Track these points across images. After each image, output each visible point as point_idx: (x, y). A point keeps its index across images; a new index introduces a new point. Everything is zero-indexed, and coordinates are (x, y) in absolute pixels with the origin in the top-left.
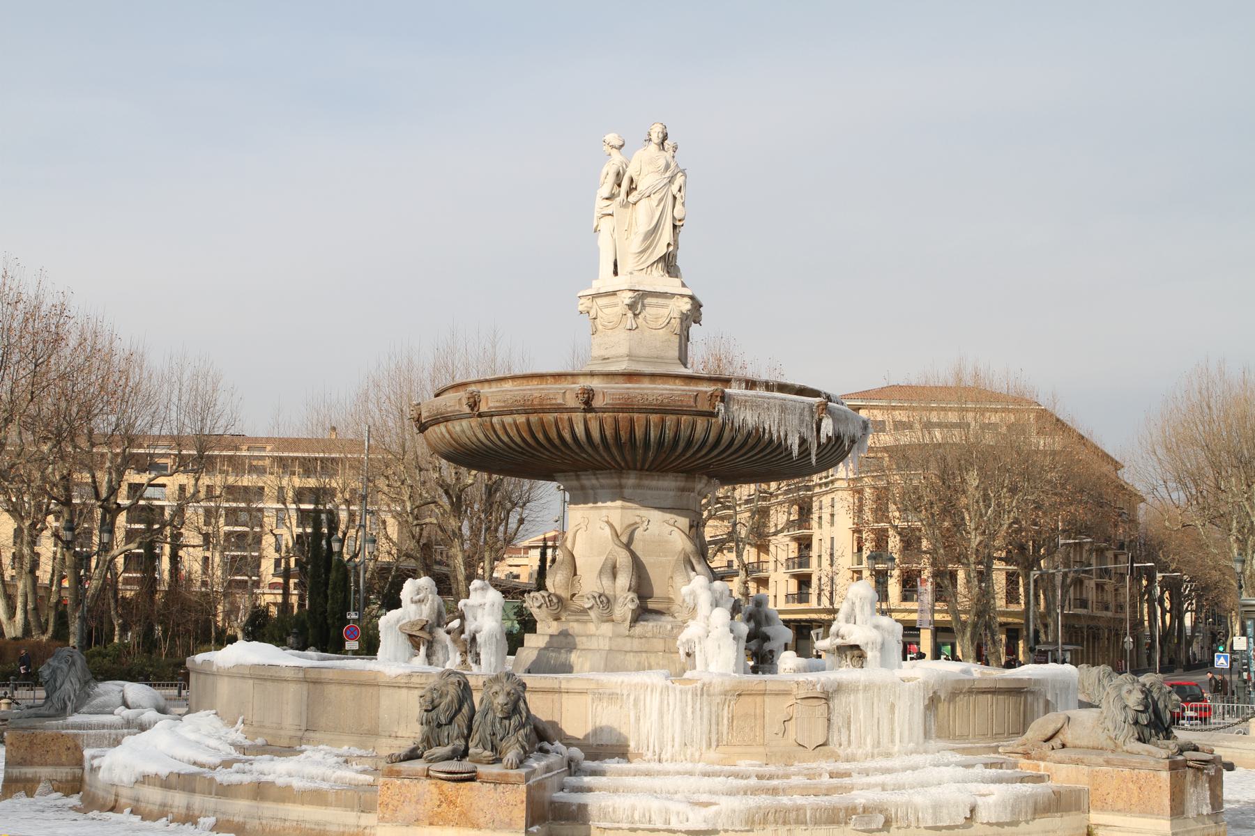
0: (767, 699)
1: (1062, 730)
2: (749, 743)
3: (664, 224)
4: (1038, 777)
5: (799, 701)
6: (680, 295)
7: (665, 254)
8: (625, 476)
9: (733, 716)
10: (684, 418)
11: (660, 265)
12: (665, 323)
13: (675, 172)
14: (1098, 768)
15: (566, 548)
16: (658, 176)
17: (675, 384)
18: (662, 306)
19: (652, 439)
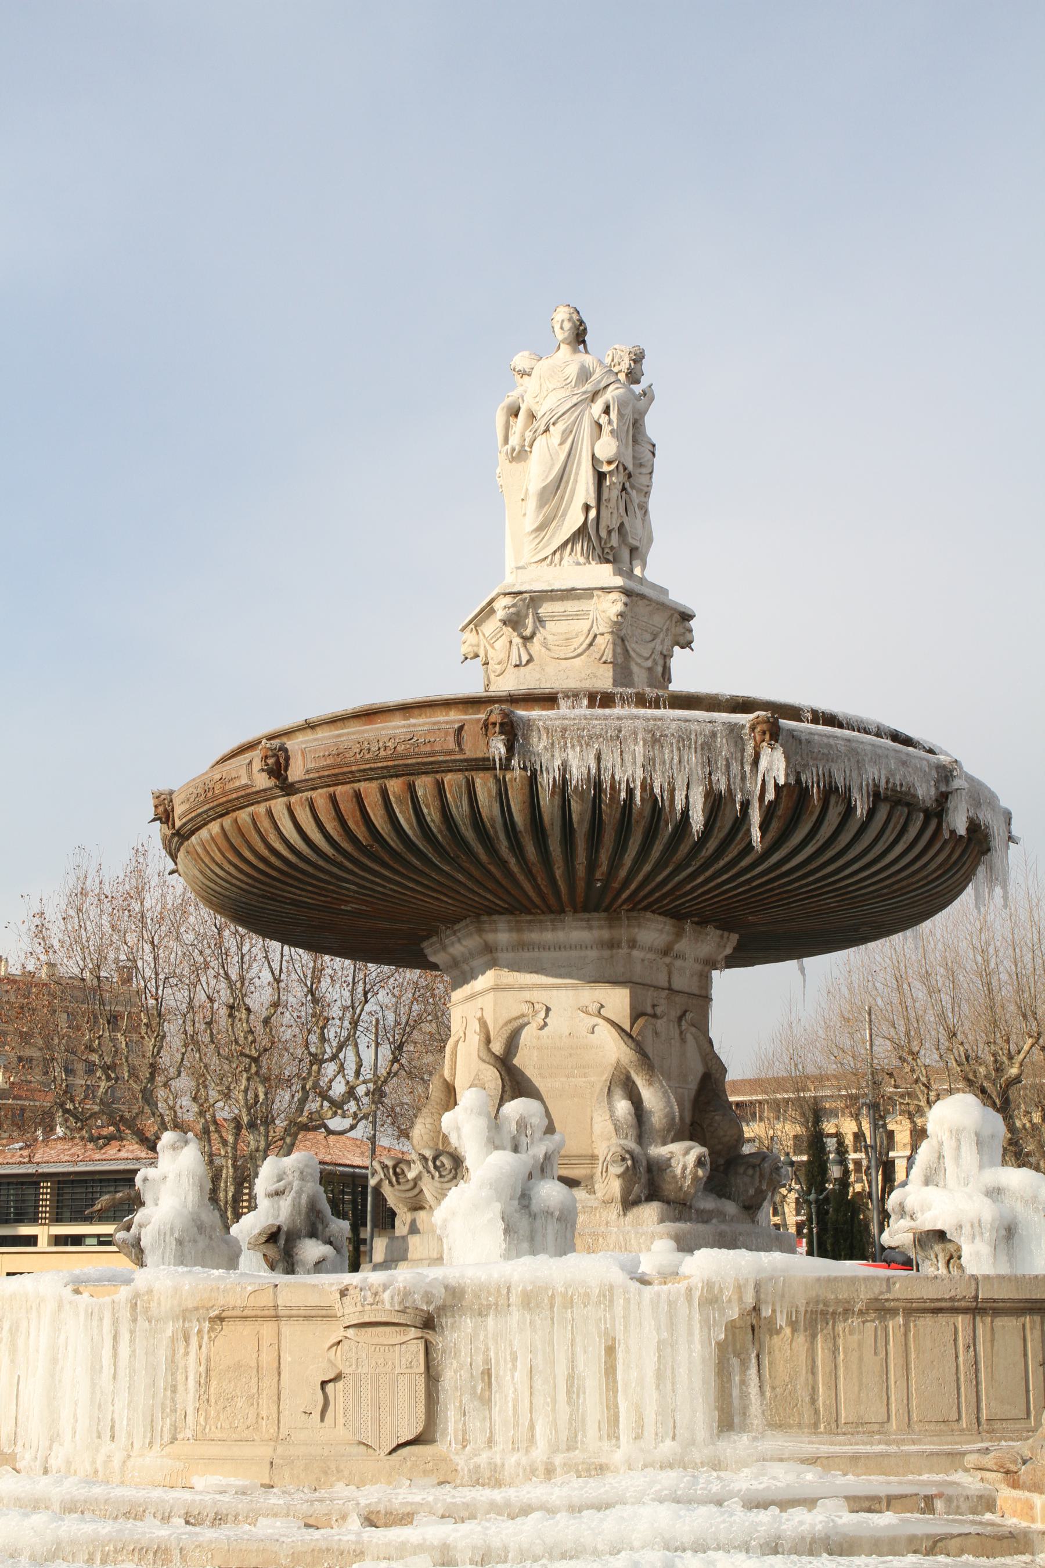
0: (288, 1329)
2: (246, 1434)
3: (577, 474)
4: (1000, 1538)
5: (351, 1332)
6: (602, 589)
8: (486, 926)
9: (208, 1370)
10: (448, 778)
11: (578, 547)
12: (584, 646)
13: (603, 384)
15: (442, 1076)
18: (577, 616)
19: (409, 832)
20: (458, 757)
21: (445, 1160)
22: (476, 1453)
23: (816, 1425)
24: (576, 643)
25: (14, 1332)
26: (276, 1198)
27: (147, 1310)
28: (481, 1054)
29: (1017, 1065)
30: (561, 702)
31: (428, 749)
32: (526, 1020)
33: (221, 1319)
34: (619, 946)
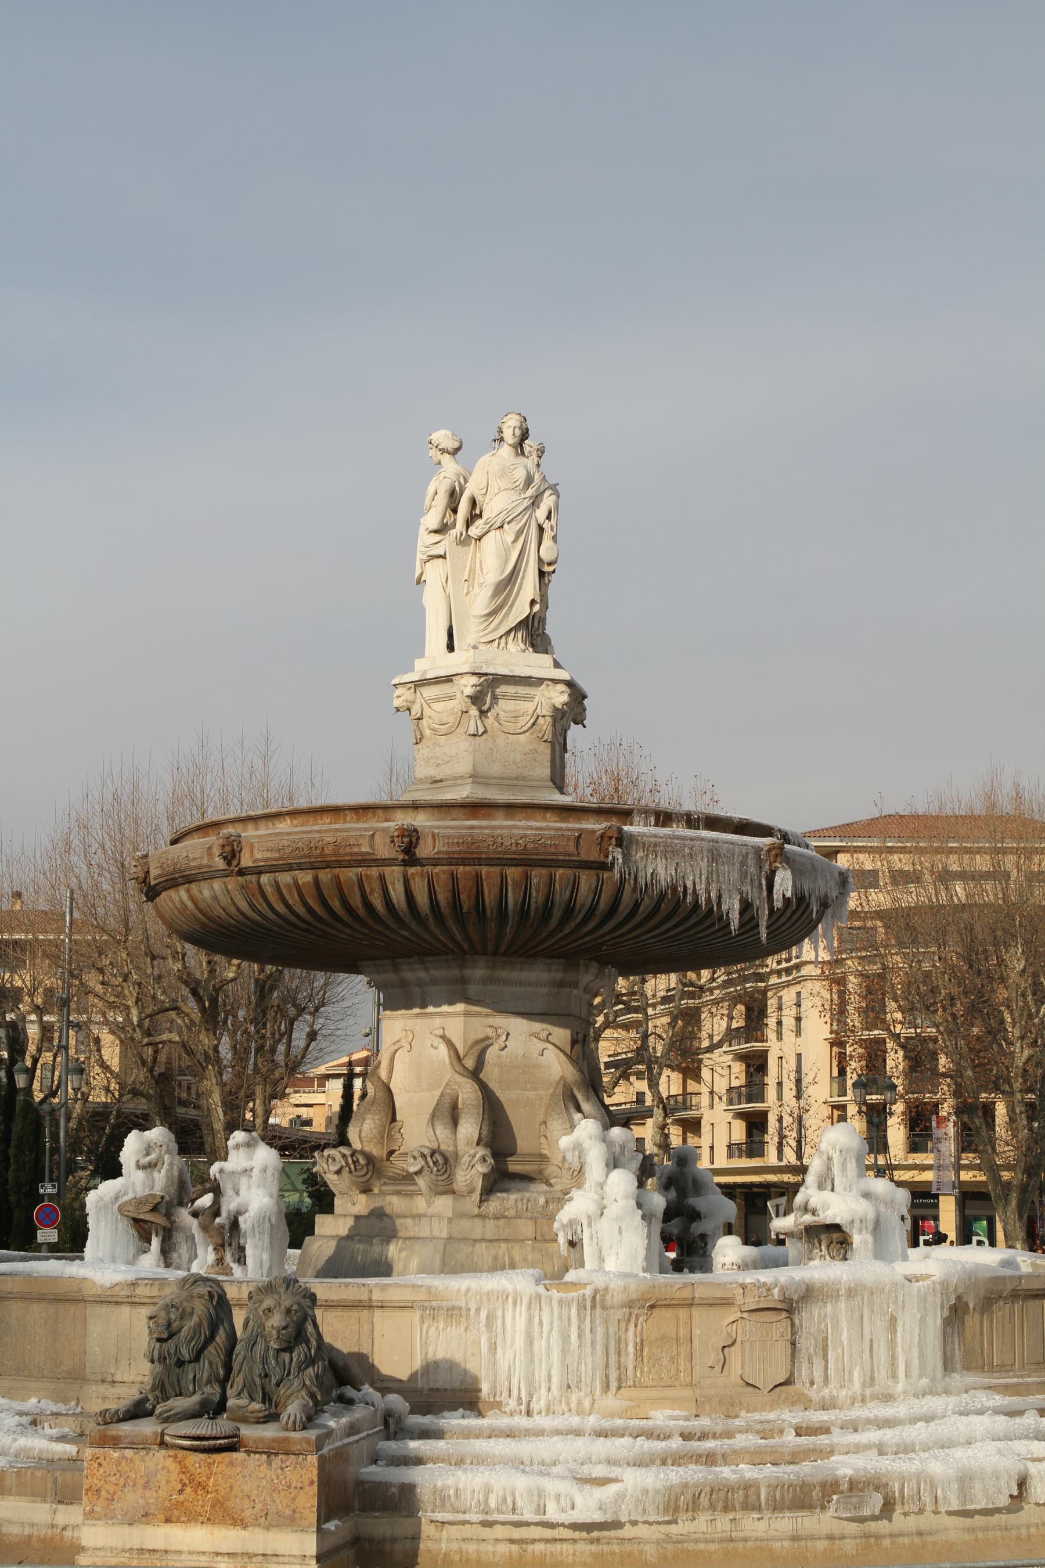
0: (696, 1312)
3: (525, 571)
5: (745, 1315)
7: (527, 617)
9: (642, 1341)
11: (520, 635)
12: (529, 725)
13: (542, 489)
15: (379, 1078)
16: (514, 496)
17: (545, 820)
18: (525, 698)
20: (574, 858)
21: (438, 1157)
22: (819, 1391)
23: (983, 1368)
24: (522, 721)
25: (490, 1318)
26: (149, 1170)
27: (603, 1300)
28: (457, 1069)
29: (234, 968)
30: (637, 818)
31: (553, 850)
32: (490, 1041)
33: (652, 1307)
34: (576, 987)
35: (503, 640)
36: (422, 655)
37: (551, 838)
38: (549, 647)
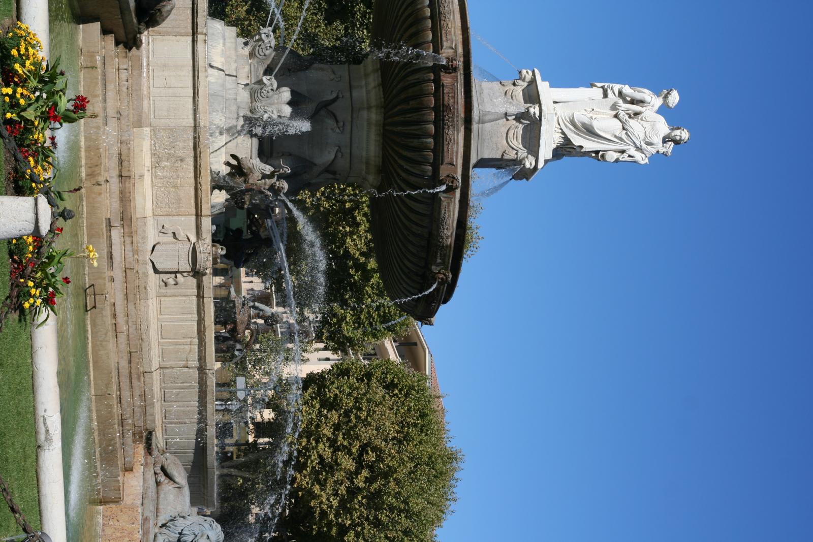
1: (172, 482)
7: (573, 144)
13: (645, 152)
14: (140, 511)
35: (560, 131)
36: (551, 86)
37: (453, 150)
38: (555, 158)
